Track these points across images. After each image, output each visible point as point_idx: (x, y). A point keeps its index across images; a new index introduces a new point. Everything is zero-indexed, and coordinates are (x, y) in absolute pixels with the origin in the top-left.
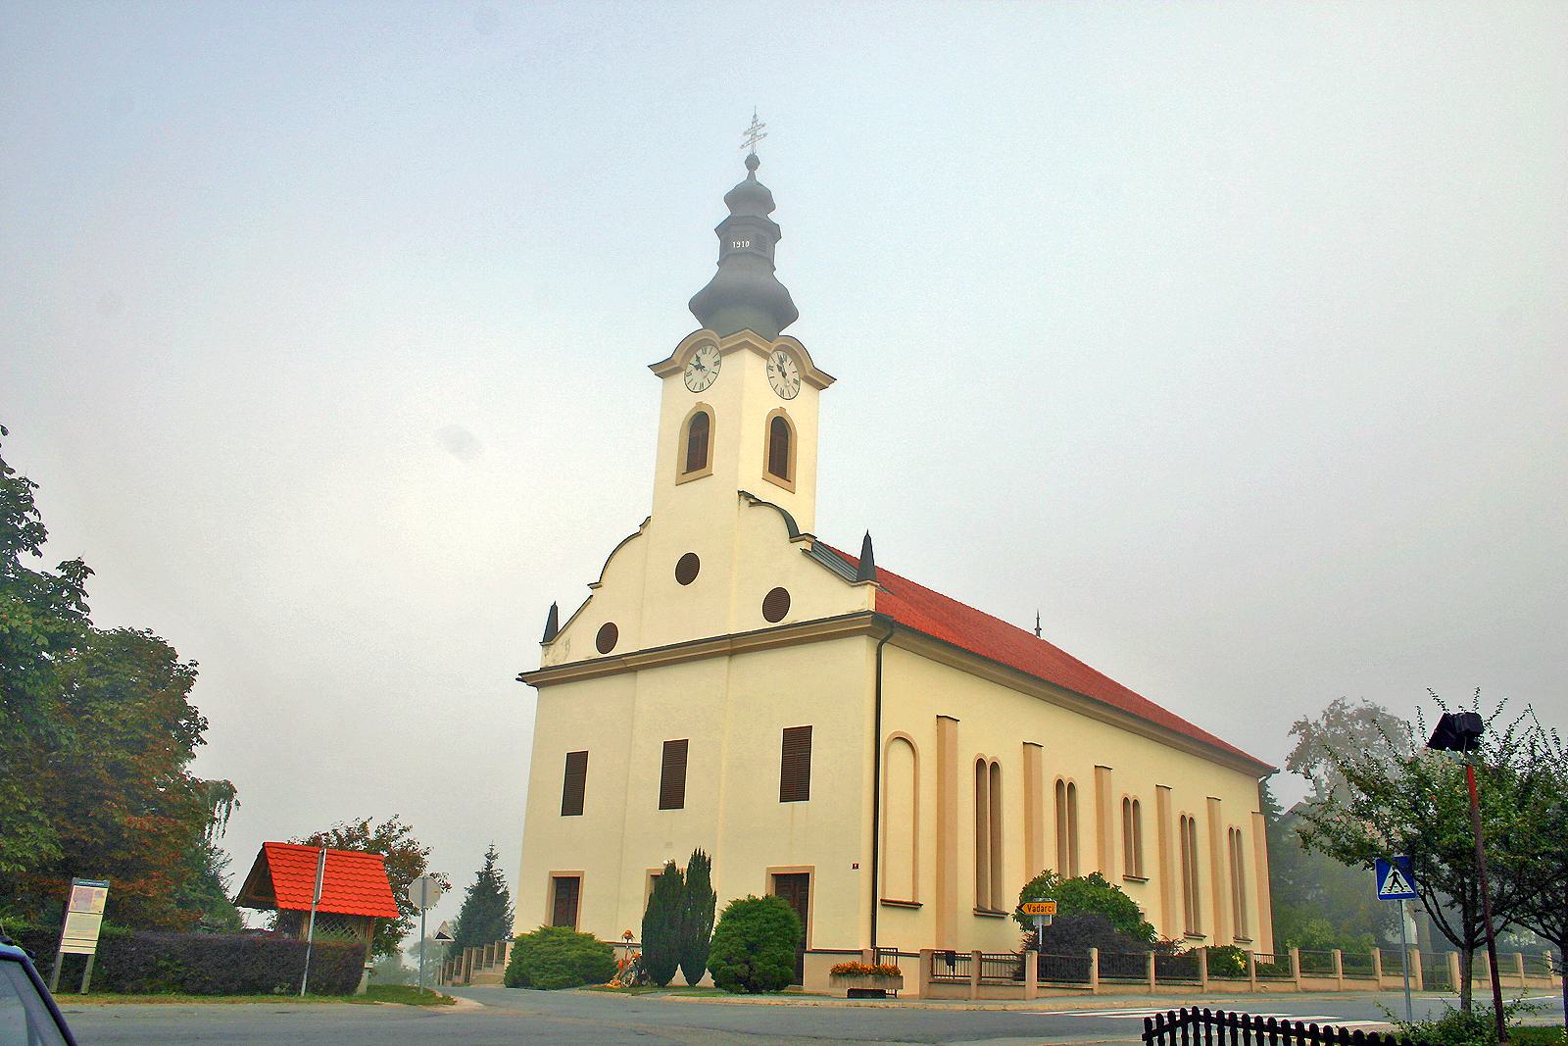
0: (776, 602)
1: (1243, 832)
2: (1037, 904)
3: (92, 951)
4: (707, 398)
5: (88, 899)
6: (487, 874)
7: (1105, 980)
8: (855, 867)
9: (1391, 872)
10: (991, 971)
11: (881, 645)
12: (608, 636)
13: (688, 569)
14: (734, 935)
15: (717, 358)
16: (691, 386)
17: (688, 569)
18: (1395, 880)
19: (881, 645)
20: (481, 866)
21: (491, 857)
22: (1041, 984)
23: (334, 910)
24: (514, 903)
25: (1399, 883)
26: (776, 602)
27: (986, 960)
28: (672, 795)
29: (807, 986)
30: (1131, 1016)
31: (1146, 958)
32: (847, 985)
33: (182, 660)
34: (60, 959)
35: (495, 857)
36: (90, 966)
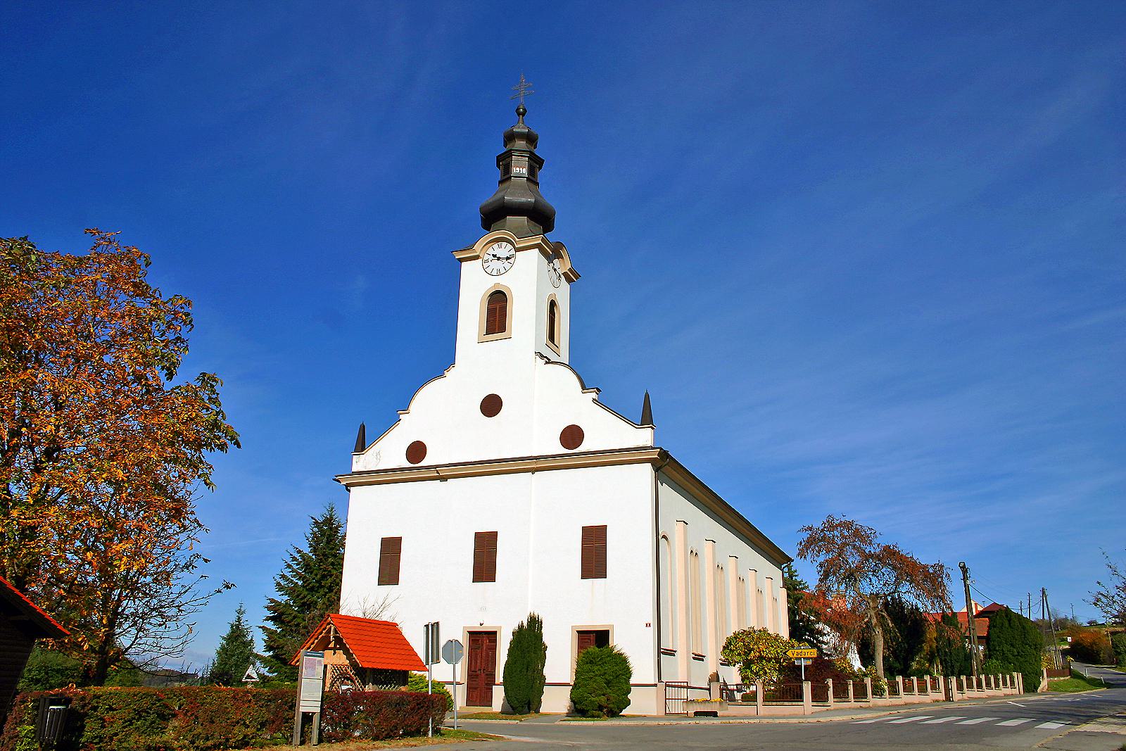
0: (572, 436)
2: (800, 651)
4: (504, 282)
5: (313, 668)
6: (237, 627)
7: (767, 703)
12: (417, 451)
13: (491, 406)
14: (596, 675)
16: (489, 270)
17: (491, 406)
20: (233, 619)
21: (240, 612)
22: (836, 700)
24: (634, 663)
26: (572, 436)
27: (669, 686)
28: (484, 568)
30: (864, 722)
31: (847, 685)
32: (695, 708)
35: (244, 612)
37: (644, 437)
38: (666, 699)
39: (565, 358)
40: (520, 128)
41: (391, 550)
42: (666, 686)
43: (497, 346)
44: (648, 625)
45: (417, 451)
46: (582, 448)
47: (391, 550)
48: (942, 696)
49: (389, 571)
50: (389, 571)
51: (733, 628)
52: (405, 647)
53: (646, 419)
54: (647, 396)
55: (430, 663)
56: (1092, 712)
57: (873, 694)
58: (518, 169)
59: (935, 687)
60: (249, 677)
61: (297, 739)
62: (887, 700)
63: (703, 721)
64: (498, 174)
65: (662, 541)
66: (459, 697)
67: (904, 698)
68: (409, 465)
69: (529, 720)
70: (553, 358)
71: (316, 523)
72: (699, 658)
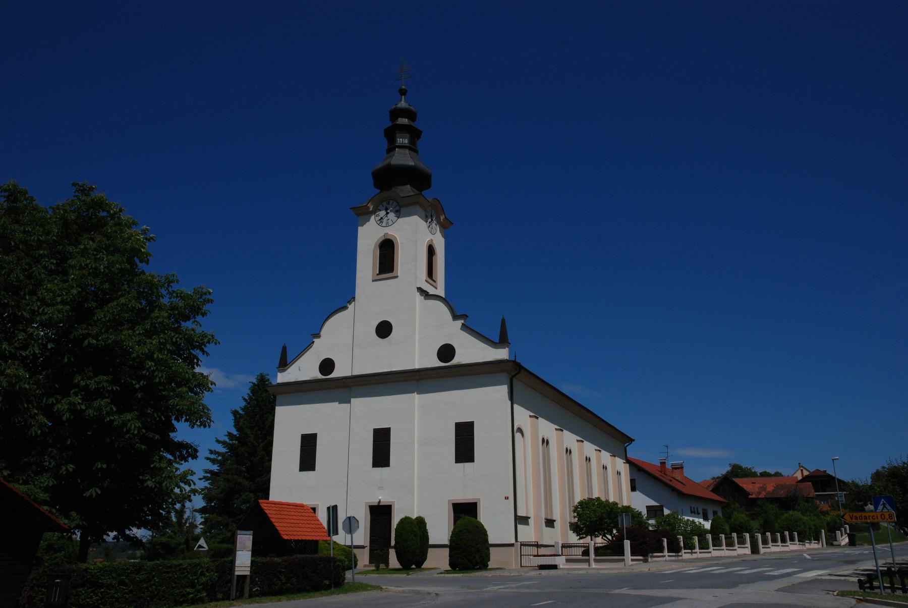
0: (446, 352)
1: (607, 467)
3: (248, 573)
8: (507, 498)
9: (882, 503)
10: (568, 552)
11: (513, 377)
12: (327, 366)
13: (384, 330)
15: (398, 208)
17: (384, 330)
18: (884, 506)
19: (513, 377)
23: (304, 538)
25: (886, 508)
26: (446, 352)
29: (491, 565)
33: (880, 469)
34: (236, 577)
36: (248, 580)
37: (502, 354)
38: (521, 555)
39: (441, 292)
40: (403, 104)
41: (309, 443)
42: (521, 545)
43: (387, 285)
44: (507, 498)
45: (327, 366)
46: (455, 361)
47: (309, 443)
48: (748, 551)
49: (308, 461)
50: (308, 461)
51: (578, 499)
52: (316, 522)
53: (502, 341)
54: (503, 321)
55: (332, 535)
56: (446, 572)
57: (714, 546)
58: (401, 140)
59: (742, 542)
60: (200, 546)
61: (233, 594)
62: (698, 554)
63: (544, 572)
64: (385, 144)
65: (518, 436)
66: (363, 558)
67: (714, 553)
68: (320, 376)
69: (415, 575)
70: (431, 291)
71: (244, 399)
72: (550, 523)
